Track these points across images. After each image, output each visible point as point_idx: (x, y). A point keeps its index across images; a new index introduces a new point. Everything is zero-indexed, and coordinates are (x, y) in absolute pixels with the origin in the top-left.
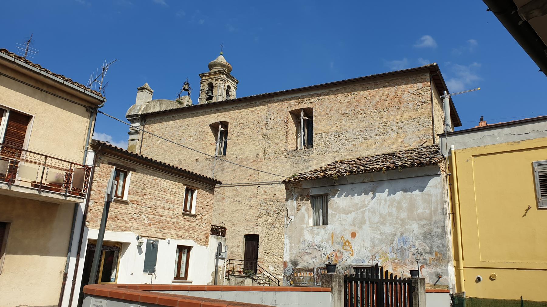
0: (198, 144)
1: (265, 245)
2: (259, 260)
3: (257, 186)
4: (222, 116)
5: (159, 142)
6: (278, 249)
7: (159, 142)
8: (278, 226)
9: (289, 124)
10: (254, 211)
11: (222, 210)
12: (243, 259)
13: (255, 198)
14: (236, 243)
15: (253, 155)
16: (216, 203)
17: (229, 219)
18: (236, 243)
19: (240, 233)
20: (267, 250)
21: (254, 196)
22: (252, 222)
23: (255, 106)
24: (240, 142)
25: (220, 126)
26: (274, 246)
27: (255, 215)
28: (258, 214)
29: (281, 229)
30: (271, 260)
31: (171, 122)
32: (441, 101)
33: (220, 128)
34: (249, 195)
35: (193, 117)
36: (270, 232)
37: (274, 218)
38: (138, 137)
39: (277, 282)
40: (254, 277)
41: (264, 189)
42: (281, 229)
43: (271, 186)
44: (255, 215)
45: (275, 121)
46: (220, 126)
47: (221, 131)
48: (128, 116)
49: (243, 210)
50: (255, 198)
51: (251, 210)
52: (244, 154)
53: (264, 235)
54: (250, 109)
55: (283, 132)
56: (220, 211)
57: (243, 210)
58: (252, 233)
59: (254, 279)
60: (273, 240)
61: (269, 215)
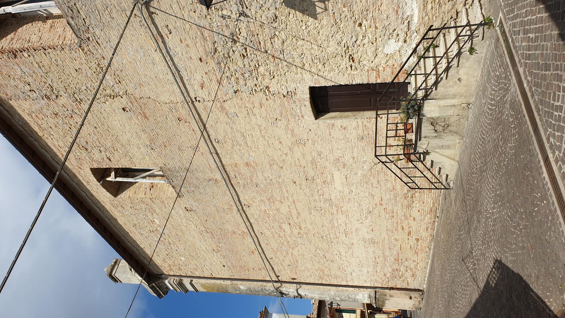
0: (158, 211)
1: (332, 70)
2: (373, 81)
3: (196, 104)
4: (87, 179)
5: (183, 258)
6: (338, 37)
7: (183, 258)
8: (277, 43)
9: (16, 46)
10: (257, 104)
11: (271, 165)
12: (372, 114)
13: (226, 105)
14: (337, 133)
15: (130, 119)
16: (260, 175)
17: (286, 150)
18: (337, 133)
19: (313, 127)
20: (345, 63)
21: (222, 107)
22: (282, 105)
23: (26, 123)
24: (118, 146)
25: (108, 179)
26: (332, 47)
27: (264, 101)
28: (261, 94)
29: (283, 35)
30: (370, 50)
31: (142, 247)
32: (557, 165)
33: (112, 178)
34: (222, 117)
35: (116, 220)
36: (298, 62)
37: (260, 57)
38: (186, 282)
39: (431, 34)
40: (421, 94)
41: (197, 87)
42: (283, 35)
43: (184, 73)
44: (264, 101)
45: (30, 80)
46: (108, 179)
47: (116, 177)
48: (159, 296)
49: (259, 126)
50: (226, 105)
51: (256, 111)
52: (139, 138)
53: (307, 76)
54: (40, 134)
55: (40, 57)
56: (275, 167)
57: (259, 126)
58: (308, 103)
59: (426, 97)
60: (316, 51)
61: (256, 68)
